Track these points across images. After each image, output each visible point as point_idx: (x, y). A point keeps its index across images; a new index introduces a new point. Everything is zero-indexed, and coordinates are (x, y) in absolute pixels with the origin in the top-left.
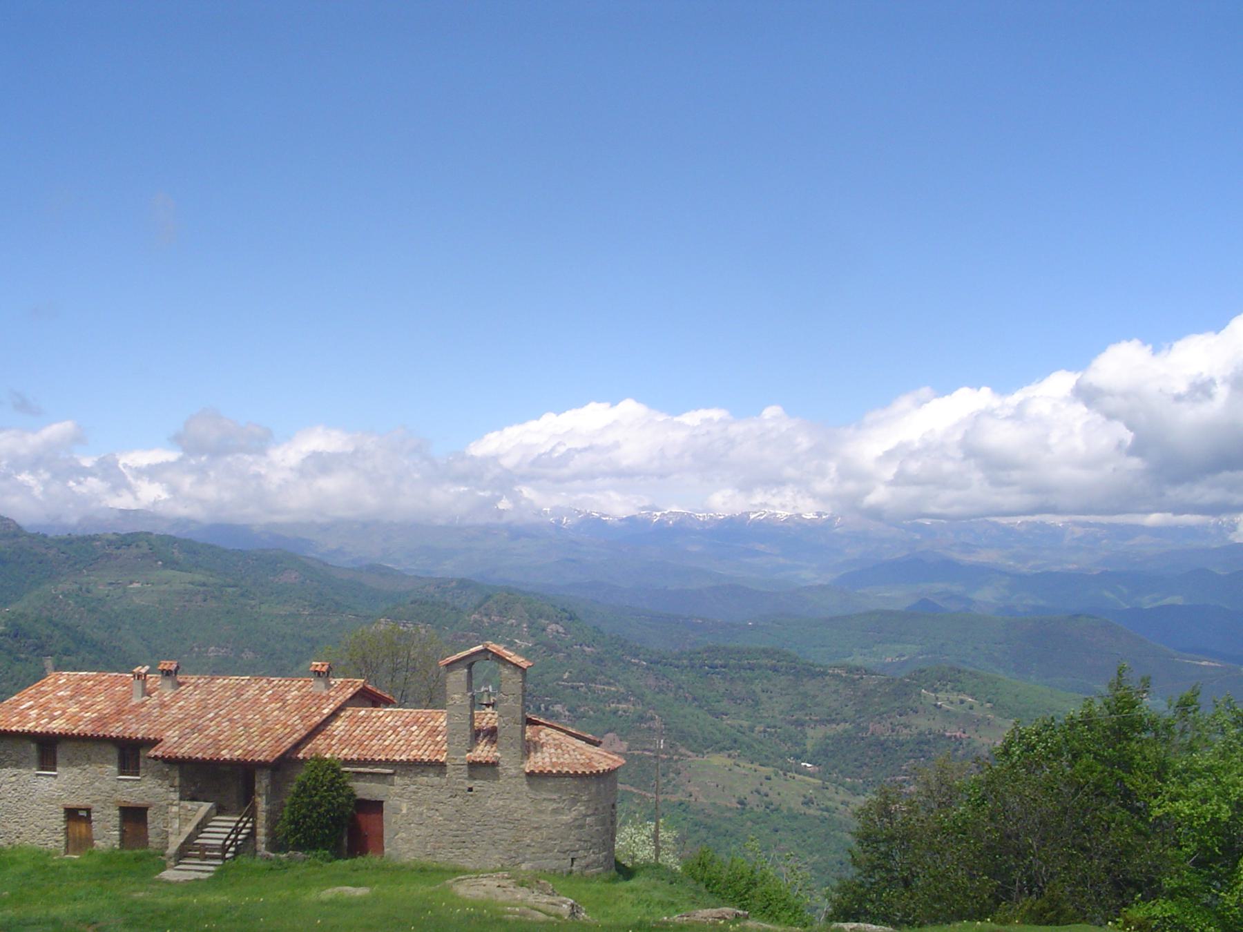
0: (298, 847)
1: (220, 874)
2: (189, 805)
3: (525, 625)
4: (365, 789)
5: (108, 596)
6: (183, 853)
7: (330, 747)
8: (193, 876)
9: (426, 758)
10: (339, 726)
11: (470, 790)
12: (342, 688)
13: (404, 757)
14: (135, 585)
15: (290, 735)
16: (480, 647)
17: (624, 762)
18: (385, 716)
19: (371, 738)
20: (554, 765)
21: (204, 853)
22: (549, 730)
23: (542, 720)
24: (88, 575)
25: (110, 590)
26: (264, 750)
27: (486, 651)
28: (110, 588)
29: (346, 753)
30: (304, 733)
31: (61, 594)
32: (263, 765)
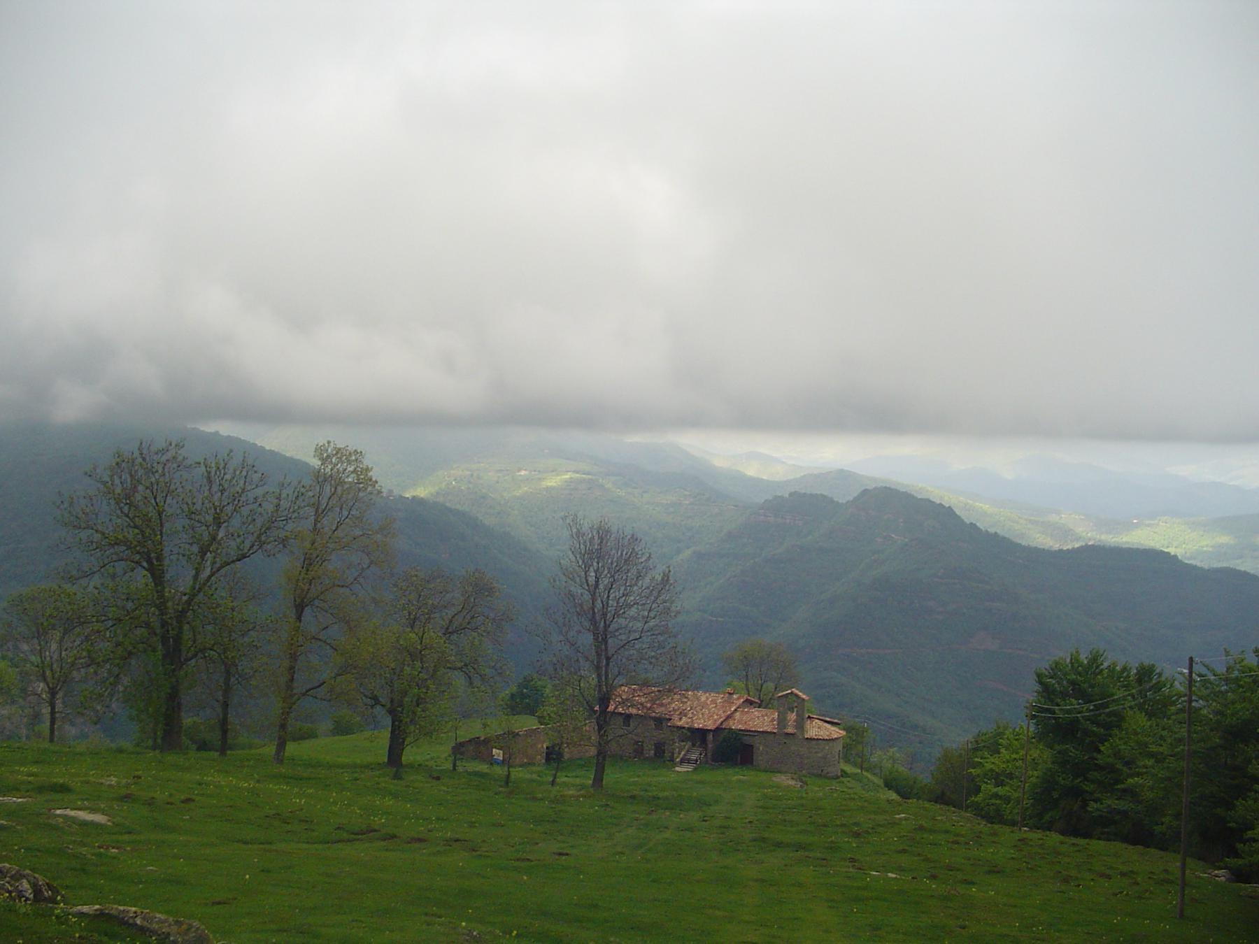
0: (722, 761)
1: (695, 769)
2: (682, 744)
3: (901, 520)
4: (747, 740)
5: (498, 482)
6: (682, 761)
7: (735, 725)
8: (686, 770)
9: (769, 730)
10: (737, 715)
11: (785, 743)
12: (738, 699)
13: (761, 730)
14: (523, 473)
15: (718, 719)
16: (789, 691)
17: (845, 733)
18: (756, 712)
19: (749, 721)
20: (816, 735)
21: (689, 761)
22: (817, 721)
23: (815, 716)
24: (479, 462)
25: (499, 477)
26: (710, 725)
27: (792, 693)
28: (500, 475)
29: (740, 727)
30: (724, 718)
31: (455, 480)
32: (711, 730)
